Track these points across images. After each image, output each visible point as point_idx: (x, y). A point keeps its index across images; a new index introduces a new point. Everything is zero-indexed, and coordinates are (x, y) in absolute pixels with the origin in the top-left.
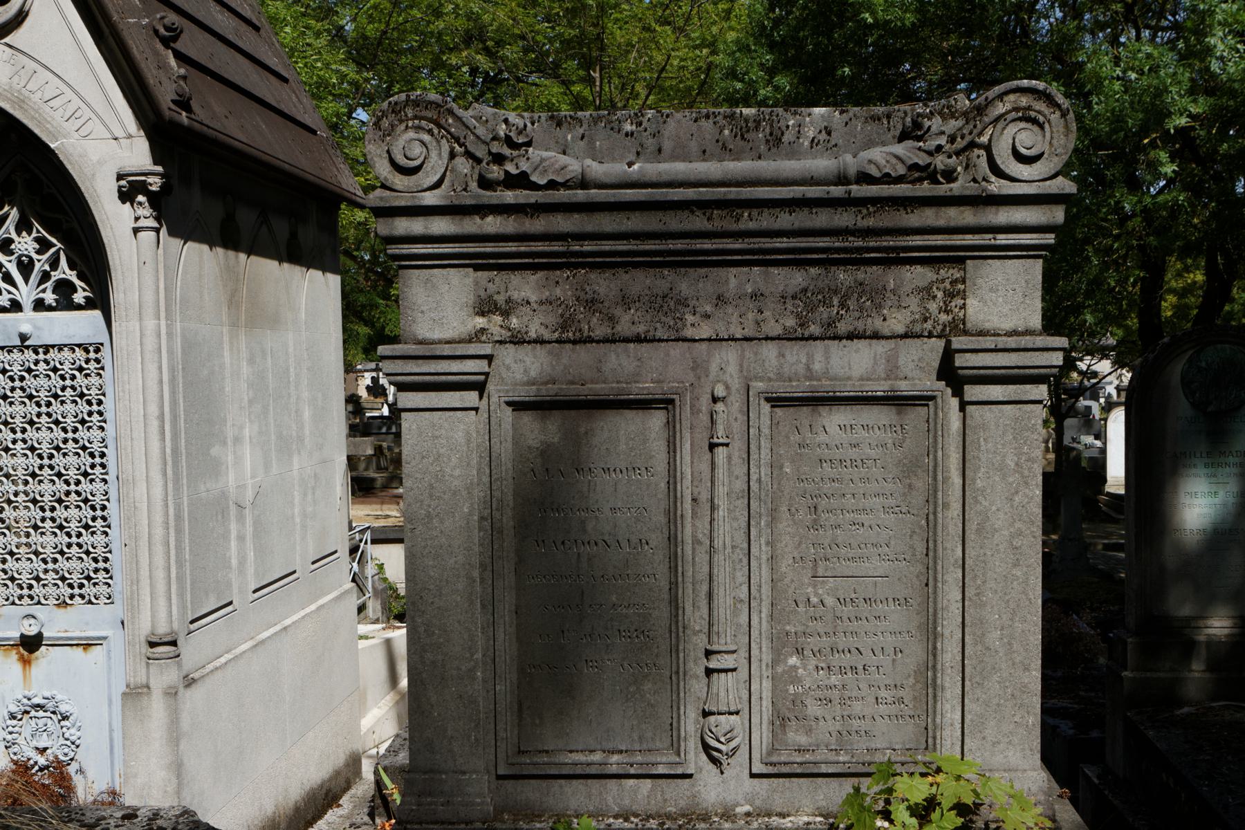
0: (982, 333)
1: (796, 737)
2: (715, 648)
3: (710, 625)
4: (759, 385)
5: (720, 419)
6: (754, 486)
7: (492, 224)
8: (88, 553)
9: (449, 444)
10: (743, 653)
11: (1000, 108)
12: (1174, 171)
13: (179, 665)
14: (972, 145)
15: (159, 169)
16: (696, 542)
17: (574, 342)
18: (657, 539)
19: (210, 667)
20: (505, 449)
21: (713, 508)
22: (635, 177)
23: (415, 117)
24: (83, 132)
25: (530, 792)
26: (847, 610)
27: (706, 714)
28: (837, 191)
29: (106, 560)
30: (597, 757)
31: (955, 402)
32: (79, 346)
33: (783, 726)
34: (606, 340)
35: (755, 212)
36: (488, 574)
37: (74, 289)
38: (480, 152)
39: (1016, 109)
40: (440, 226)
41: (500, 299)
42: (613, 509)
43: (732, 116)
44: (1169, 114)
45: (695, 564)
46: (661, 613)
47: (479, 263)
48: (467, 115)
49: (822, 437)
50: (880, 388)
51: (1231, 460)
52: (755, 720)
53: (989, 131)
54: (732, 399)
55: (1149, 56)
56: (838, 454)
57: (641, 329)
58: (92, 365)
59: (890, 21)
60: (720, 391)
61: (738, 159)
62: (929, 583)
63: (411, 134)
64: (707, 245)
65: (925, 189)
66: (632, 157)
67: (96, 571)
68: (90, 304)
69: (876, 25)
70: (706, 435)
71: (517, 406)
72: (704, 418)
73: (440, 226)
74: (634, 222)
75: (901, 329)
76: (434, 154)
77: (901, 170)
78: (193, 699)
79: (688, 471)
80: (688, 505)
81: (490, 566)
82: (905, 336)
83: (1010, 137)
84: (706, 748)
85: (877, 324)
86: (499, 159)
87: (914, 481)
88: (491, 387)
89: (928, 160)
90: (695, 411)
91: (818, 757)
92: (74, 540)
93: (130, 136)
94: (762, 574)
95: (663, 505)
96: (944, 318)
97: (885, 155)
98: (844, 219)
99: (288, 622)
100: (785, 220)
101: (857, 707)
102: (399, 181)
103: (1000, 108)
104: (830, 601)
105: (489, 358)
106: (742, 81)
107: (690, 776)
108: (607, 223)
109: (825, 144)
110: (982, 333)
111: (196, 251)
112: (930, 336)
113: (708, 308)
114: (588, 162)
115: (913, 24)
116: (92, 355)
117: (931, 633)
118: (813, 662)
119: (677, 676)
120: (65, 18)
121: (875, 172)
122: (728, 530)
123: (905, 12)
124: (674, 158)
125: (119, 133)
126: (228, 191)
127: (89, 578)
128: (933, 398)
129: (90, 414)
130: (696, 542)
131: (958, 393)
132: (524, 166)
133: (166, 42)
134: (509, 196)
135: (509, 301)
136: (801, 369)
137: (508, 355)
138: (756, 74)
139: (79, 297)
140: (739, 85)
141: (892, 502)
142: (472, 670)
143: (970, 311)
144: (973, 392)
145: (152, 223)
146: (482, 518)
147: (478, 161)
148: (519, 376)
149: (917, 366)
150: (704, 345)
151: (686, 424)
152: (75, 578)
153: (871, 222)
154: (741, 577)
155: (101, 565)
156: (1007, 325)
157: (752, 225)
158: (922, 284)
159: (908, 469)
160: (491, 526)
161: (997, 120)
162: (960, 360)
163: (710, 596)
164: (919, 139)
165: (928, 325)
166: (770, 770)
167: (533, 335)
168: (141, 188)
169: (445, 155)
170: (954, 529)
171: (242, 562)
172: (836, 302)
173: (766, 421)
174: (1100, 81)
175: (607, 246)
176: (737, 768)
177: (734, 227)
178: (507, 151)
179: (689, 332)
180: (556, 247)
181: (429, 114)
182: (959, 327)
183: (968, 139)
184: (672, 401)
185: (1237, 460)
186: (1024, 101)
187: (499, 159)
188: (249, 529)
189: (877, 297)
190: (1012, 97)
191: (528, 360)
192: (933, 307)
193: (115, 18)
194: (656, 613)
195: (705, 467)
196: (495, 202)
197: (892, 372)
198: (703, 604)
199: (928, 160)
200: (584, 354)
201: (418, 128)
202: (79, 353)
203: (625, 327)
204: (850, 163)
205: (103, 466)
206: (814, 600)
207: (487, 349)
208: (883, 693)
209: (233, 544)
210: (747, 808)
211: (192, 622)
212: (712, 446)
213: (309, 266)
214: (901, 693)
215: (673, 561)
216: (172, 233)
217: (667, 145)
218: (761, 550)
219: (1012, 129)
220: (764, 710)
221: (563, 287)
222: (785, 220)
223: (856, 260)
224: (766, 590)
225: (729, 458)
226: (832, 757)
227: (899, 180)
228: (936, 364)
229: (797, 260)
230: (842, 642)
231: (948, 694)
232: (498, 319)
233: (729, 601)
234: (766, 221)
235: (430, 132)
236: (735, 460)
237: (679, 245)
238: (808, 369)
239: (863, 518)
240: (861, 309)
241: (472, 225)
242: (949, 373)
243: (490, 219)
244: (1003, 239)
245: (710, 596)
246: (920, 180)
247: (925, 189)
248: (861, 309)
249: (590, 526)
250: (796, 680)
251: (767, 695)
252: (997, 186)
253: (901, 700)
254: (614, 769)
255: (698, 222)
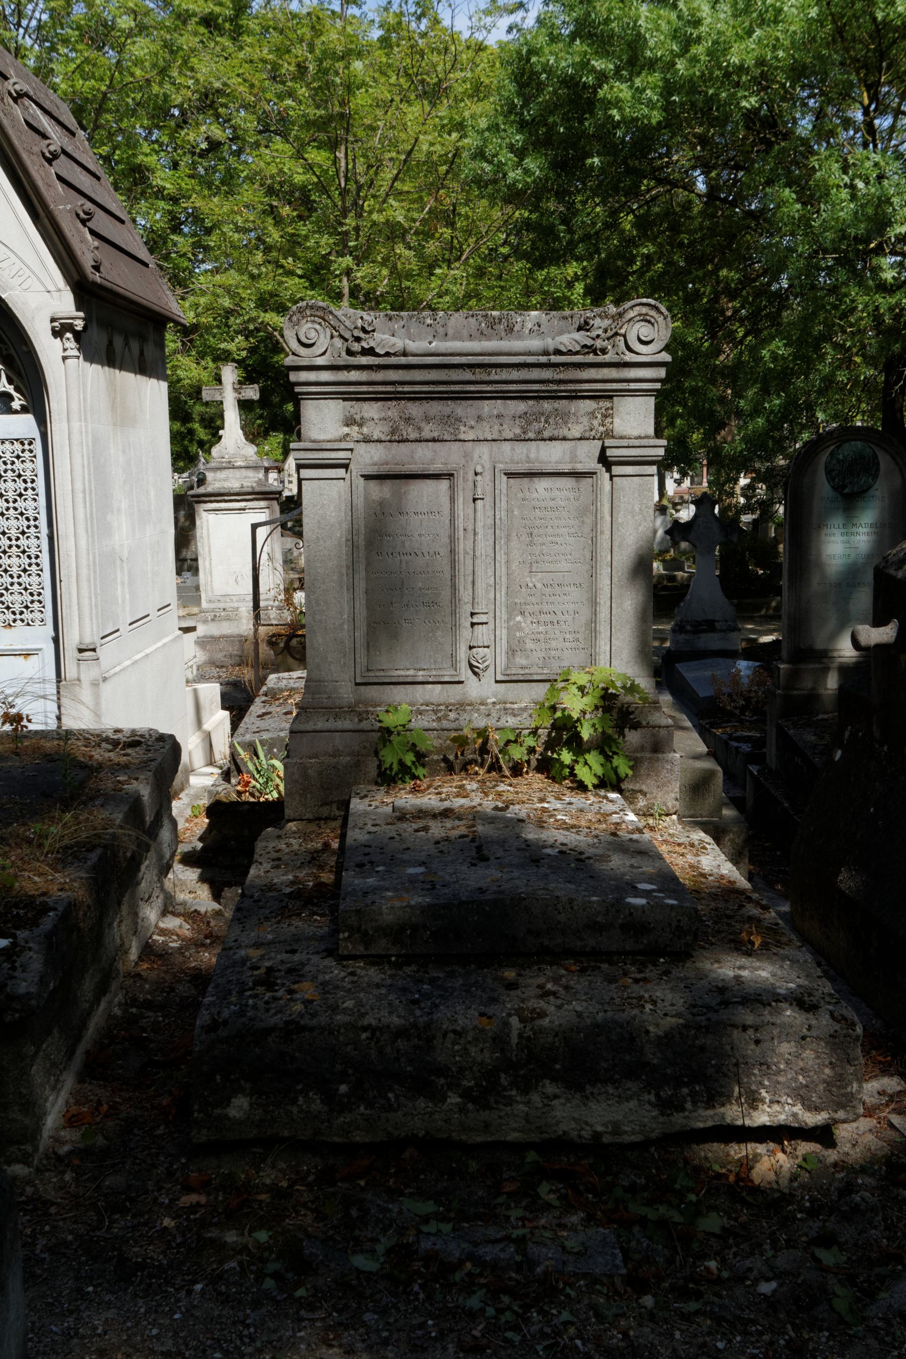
0: (621, 438)
1: (520, 660)
2: (476, 611)
3: (473, 599)
4: (500, 466)
5: (479, 484)
6: (498, 521)
7: (354, 376)
8: (26, 589)
9: (328, 502)
10: (491, 614)
11: (631, 314)
12: (894, 278)
13: (99, 664)
14: (616, 334)
15: (81, 314)
16: (466, 553)
17: (399, 442)
18: (444, 552)
19: (118, 669)
20: (360, 502)
21: (475, 534)
22: (433, 351)
23: (311, 315)
24: (24, 286)
25: (372, 692)
26: (548, 590)
27: (471, 648)
28: (543, 359)
29: (39, 594)
30: (411, 672)
31: (607, 475)
32: (17, 440)
33: (513, 655)
34: (416, 441)
35: (498, 370)
36: (351, 571)
37: (11, 398)
38: (347, 335)
39: (640, 315)
40: (325, 376)
41: (357, 417)
42: (420, 535)
43: (486, 316)
44: (890, 224)
45: (465, 566)
46: (446, 593)
47: (346, 397)
48: (339, 313)
49: (535, 495)
50: (566, 468)
51: (861, 530)
52: (498, 651)
53: (625, 326)
54: (486, 473)
55: (876, 164)
56: (543, 504)
57: (435, 434)
58: (27, 454)
59: (637, 119)
60: (479, 470)
61: (489, 340)
62: (593, 575)
63: (309, 325)
64: (472, 388)
65: (591, 358)
66: (431, 339)
67: (32, 602)
68: (24, 410)
69: (624, 120)
70: (471, 494)
71: (367, 477)
72: (470, 484)
73: (325, 376)
74: (433, 375)
75: (578, 435)
76: (322, 336)
77: (578, 348)
78: (106, 689)
79: (461, 514)
80: (461, 532)
81: (352, 567)
82: (581, 439)
83: (636, 330)
84: (471, 666)
85: (564, 432)
86: (358, 339)
87: (585, 519)
88: (352, 466)
89: (592, 342)
90: (465, 480)
91: (532, 671)
92: (16, 580)
93: (59, 290)
94: (502, 570)
95: (448, 532)
96: (601, 429)
97: (570, 339)
98: (547, 374)
99: (148, 651)
100: (515, 375)
101: (554, 644)
102: (302, 351)
103: (631, 314)
104: (539, 585)
105: (351, 450)
106: (490, 162)
107: (462, 682)
108: (418, 375)
109: (537, 333)
110: (621, 438)
111: (96, 368)
112: (594, 439)
113: (473, 423)
114: (407, 341)
115: (659, 123)
116: (27, 447)
117: (594, 603)
118: (530, 619)
119: (455, 627)
120: (9, 202)
121: (564, 350)
122: (484, 546)
123: (652, 109)
124: (455, 338)
125: (51, 288)
126: (117, 328)
127: (27, 607)
128: (595, 473)
129: (26, 489)
130: (466, 553)
131: (609, 470)
132: (372, 344)
133: (84, 222)
134: (364, 360)
135: (362, 418)
136: (524, 457)
137: (362, 448)
138: (506, 157)
139: (16, 405)
140: (488, 168)
141: (573, 531)
142: (342, 625)
143: (615, 425)
144: (616, 470)
145: (75, 353)
146: (347, 540)
147: (346, 340)
148: (368, 461)
149: (587, 456)
150: (471, 444)
151: (460, 487)
152: (17, 607)
153: (561, 376)
154: (490, 572)
155: (36, 598)
156: (636, 433)
157: (497, 378)
158: (591, 410)
159: (582, 512)
160: (353, 545)
161: (630, 320)
162: (609, 452)
163: (473, 583)
164: (588, 330)
165: (593, 433)
166: (506, 678)
167: (375, 437)
168: (69, 328)
169: (329, 336)
170: (606, 545)
171: (124, 601)
172: (543, 420)
173: (504, 486)
174: (828, 189)
175: (417, 388)
176: (488, 677)
177: (487, 378)
178: (362, 335)
179: (462, 436)
180: (389, 388)
181: (319, 313)
182: (609, 434)
183: (614, 331)
184: (452, 475)
185: (865, 530)
186: (644, 310)
187: (358, 339)
188: (126, 578)
189: (565, 417)
190: (638, 308)
191: (373, 451)
192: (596, 423)
193: (52, 207)
194: (443, 593)
195: (470, 511)
196: (356, 363)
197: (574, 458)
198: (470, 587)
199: (592, 342)
200: (404, 448)
201: (314, 321)
202: (17, 446)
203: (426, 434)
204: (550, 343)
205: (36, 527)
206: (530, 585)
207: (351, 445)
208: (568, 636)
209: (119, 587)
210: (494, 700)
211: (103, 638)
212: (475, 500)
213: (150, 377)
214: (578, 636)
215: (453, 563)
216: (85, 359)
217: (451, 332)
218: (501, 557)
219: (638, 325)
220: (502, 646)
221: (393, 410)
222: (515, 375)
223: (554, 397)
224: (504, 579)
225: (484, 506)
226: (540, 671)
227: (577, 353)
228: (597, 454)
229: (522, 397)
230: (546, 608)
231: (603, 636)
232: (356, 428)
233: (484, 585)
234: (504, 375)
235: (320, 324)
236: (488, 507)
237: (457, 388)
238: (528, 457)
239: (557, 539)
240: (557, 424)
241: (343, 376)
242: (604, 460)
243: (353, 372)
244: (633, 386)
245: (473, 583)
246: (588, 353)
247: (591, 358)
248: (557, 424)
249: (407, 544)
250: (520, 629)
251: (504, 637)
252: (629, 357)
253: (578, 640)
254: (420, 679)
255: (467, 375)
